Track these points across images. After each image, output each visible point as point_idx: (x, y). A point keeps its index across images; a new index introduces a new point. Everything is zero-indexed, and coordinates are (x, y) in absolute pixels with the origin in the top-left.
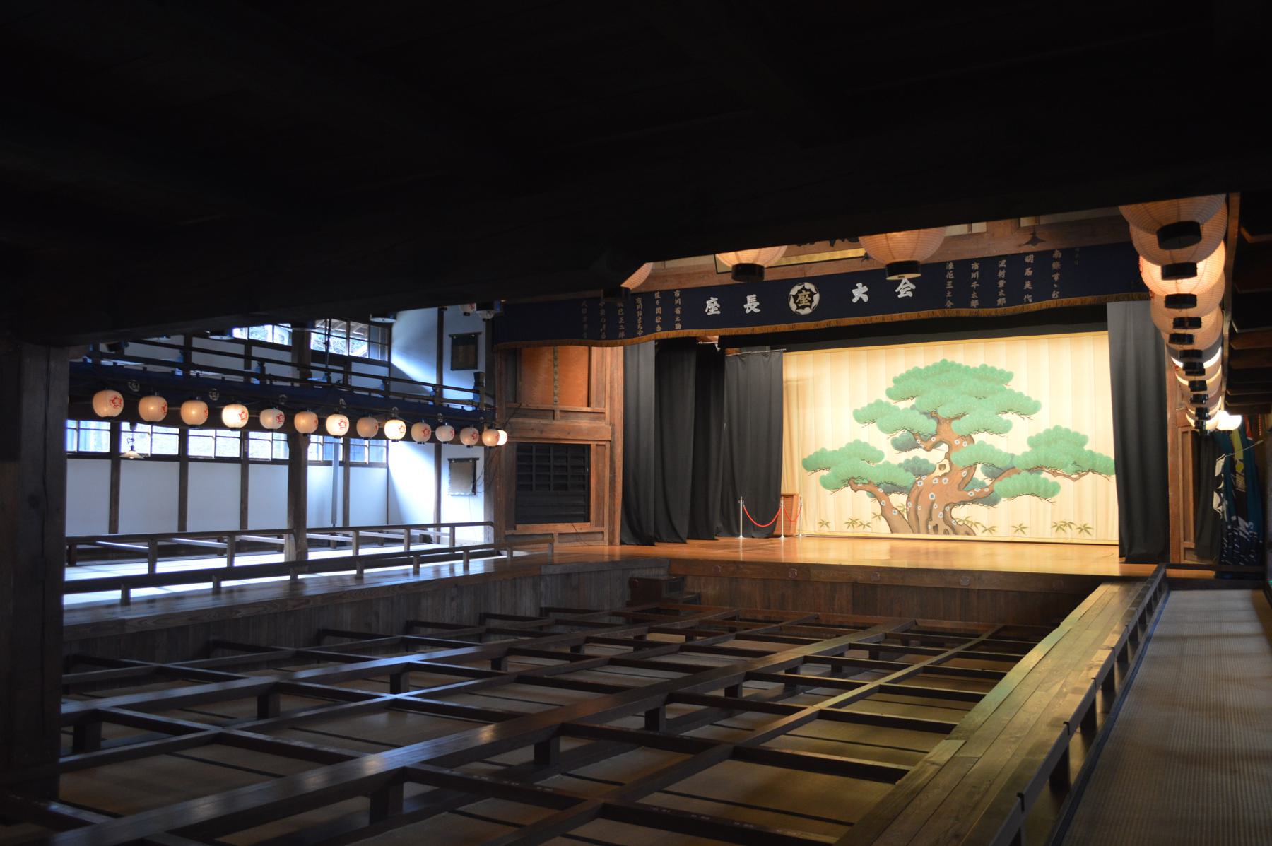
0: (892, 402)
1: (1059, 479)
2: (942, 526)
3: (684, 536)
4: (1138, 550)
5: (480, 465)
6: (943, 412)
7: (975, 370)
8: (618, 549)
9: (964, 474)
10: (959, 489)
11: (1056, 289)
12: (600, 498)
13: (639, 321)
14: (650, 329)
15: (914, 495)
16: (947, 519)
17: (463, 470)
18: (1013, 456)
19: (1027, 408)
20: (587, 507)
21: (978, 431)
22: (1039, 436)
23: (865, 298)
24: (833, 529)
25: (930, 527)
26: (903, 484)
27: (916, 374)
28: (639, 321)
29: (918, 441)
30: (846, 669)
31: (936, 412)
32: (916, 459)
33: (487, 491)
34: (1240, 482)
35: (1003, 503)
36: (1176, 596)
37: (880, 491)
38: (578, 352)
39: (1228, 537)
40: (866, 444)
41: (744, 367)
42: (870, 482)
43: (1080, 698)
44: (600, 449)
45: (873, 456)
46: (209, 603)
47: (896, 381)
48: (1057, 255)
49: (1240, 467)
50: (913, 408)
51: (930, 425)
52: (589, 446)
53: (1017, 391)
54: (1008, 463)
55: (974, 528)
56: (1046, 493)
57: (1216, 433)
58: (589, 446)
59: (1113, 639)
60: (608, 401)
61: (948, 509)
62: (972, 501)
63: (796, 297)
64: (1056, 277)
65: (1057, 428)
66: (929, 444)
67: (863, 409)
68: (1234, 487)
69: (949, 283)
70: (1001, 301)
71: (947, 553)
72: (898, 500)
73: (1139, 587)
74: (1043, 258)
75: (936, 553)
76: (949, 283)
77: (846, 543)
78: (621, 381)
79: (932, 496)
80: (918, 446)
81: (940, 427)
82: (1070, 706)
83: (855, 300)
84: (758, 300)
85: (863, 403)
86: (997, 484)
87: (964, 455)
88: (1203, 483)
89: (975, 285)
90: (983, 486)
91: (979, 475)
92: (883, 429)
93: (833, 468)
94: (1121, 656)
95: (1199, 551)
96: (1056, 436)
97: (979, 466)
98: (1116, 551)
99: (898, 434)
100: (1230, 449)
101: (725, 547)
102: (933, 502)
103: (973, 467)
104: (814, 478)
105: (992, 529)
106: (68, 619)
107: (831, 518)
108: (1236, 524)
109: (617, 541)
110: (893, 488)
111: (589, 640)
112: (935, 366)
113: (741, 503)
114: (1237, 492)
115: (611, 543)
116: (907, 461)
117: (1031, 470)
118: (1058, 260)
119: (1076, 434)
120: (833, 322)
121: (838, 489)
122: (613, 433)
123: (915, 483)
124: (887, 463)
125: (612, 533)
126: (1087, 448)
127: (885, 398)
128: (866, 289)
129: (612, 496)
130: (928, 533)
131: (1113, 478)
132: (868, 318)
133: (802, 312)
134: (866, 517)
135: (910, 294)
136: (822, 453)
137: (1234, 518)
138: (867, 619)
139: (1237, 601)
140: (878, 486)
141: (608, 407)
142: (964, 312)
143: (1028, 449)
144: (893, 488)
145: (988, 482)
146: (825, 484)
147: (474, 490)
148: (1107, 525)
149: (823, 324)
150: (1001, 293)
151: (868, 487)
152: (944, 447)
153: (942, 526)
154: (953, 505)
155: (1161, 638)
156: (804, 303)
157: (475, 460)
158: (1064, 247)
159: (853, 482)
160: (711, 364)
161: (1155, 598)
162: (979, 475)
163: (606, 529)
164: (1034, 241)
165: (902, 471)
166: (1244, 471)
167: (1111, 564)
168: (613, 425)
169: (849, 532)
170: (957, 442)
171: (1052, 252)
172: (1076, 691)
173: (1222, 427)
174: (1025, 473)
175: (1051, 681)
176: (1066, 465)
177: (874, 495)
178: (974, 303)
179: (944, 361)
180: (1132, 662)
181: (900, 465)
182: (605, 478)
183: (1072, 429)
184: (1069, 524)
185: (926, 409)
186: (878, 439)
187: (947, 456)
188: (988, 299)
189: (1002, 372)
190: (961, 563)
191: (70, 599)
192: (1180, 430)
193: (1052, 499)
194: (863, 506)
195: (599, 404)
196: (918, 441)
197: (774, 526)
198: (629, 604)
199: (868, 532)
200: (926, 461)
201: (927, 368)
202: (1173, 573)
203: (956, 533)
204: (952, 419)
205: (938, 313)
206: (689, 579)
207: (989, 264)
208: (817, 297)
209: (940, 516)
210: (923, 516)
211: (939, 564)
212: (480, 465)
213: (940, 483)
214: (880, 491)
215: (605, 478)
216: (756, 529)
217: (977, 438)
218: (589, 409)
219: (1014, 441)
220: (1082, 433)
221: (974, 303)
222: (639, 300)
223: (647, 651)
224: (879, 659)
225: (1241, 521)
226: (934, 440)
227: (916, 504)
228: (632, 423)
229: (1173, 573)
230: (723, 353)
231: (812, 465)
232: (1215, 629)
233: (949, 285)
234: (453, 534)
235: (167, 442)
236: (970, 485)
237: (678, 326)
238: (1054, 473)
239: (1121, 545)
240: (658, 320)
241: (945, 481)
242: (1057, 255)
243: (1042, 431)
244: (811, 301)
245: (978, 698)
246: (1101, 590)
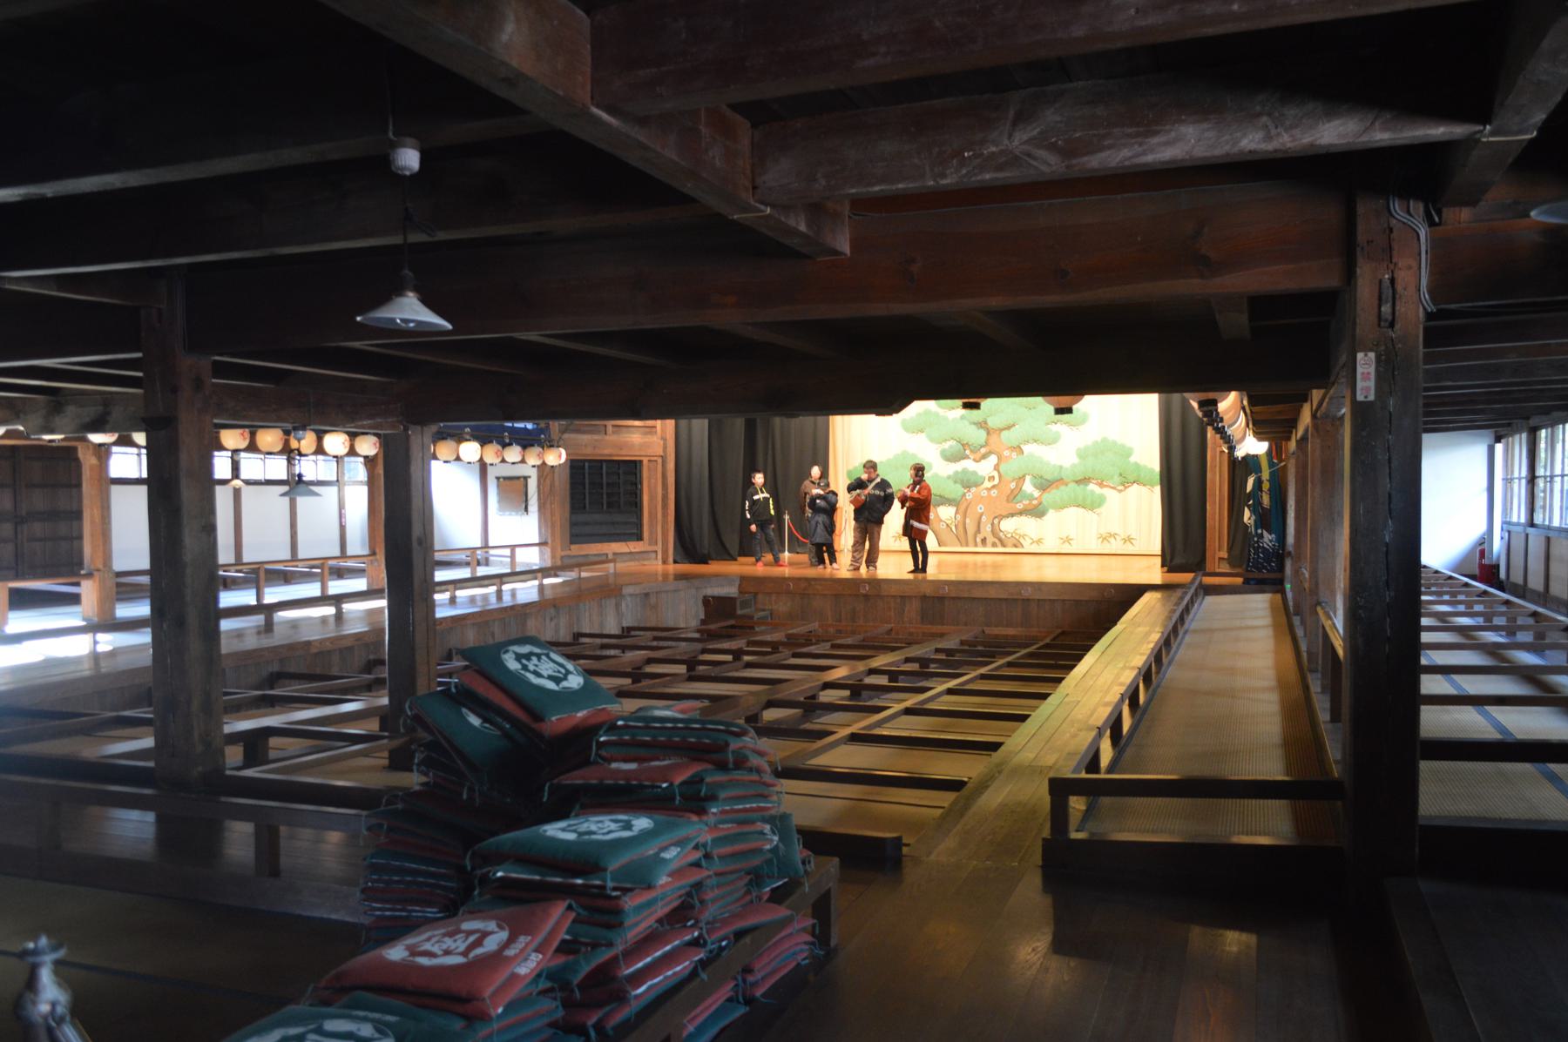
1: (1106, 491)
2: (991, 539)
3: (734, 550)
4: (1178, 560)
5: (533, 485)
8: (672, 568)
9: (1013, 485)
15: (962, 508)
16: (995, 532)
17: (514, 491)
20: (640, 525)
26: (952, 496)
30: (865, 694)
32: (965, 471)
33: (541, 507)
34: (1266, 500)
35: (1051, 514)
36: (1209, 600)
43: (1109, 709)
46: (331, 632)
49: (1266, 486)
51: (981, 436)
56: (1092, 505)
57: (1247, 458)
59: (1156, 636)
62: (1021, 513)
65: (1105, 440)
66: (978, 456)
68: (1261, 504)
71: (995, 566)
73: (1179, 593)
75: (984, 566)
79: (980, 508)
80: (967, 457)
82: (1103, 714)
87: (1012, 467)
88: (1236, 498)
90: (1031, 498)
91: (1028, 487)
92: (932, 440)
94: (1167, 643)
95: (1231, 561)
96: (1103, 448)
98: (1159, 560)
99: (946, 445)
100: (1258, 470)
103: (1023, 478)
105: (1039, 542)
106: (226, 647)
108: (1261, 536)
111: (650, 661)
113: (787, 517)
115: (665, 562)
117: (1078, 482)
122: (665, 448)
125: (665, 552)
126: (1132, 459)
129: (665, 515)
131: (1158, 489)
138: (945, 628)
139: (1259, 604)
143: (1076, 460)
145: (1036, 494)
147: (526, 509)
148: (1152, 539)
152: (993, 459)
153: (991, 539)
154: (1001, 517)
155: (1195, 631)
157: (526, 478)
161: (1192, 601)
162: (1028, 487)
163: (659, 548)
165: (951, 482)
167: (1153, 573)
168: (664, 439)
170: (1006, 453)
172: (1106, 704)
173: (1252, 452)
175: (1101, 678)
180: (1165, 660)
184: (1114, 536)
187: (996, 468)
190: (1008, 575)
191: (226, 625)
198: (703, 622)
200: (975, 473)
202: (1208, 580)
203: (1004, 546)
206: (760, 597)
209: (989, 528)
210: (971, 529)
211: (987, 576)
212: (533, 485)
217: (1026, 448)
223: (645, 683)
224: (952, 662)
227: (965, 516)
228: (684, 436)
229: (1208, 580)
232: (1238, 623)
234: (513, 556)
235: (277, 468)
238: (1101, 485)
239: (1163, 555)
241: (994, 493)
245: (1060, 680)
246: (1148, 597)
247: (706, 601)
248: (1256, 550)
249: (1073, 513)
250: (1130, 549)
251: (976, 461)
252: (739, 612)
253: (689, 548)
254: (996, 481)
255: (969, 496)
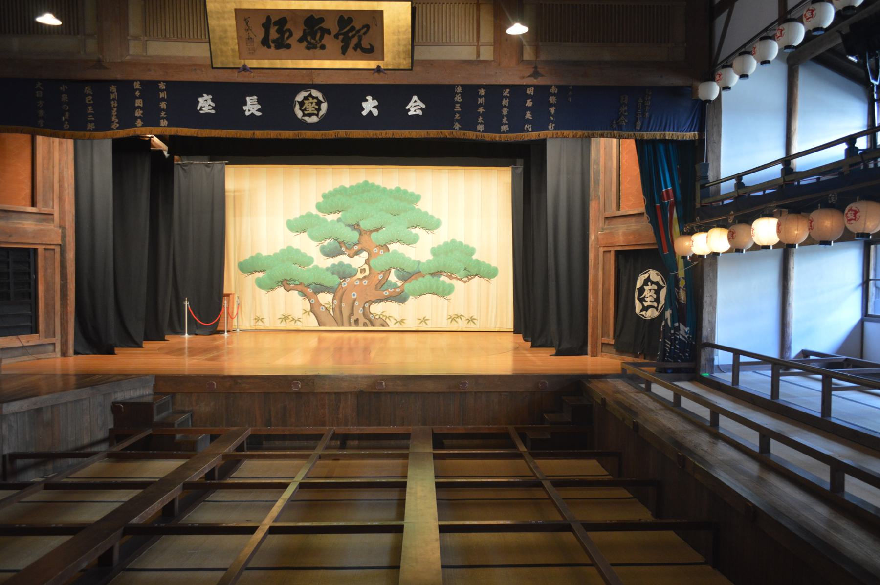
0: (321, 215)
1: (454, 282)
2: (362, 320)
4: (565, 345)
6: (365, 225)
7: (391, 191)
9: (380, 276)
10: (376, 289)
11: (552, 122)
12: (50, 307)
13: (114, 112)
14: (103, 125)
15: (339, 294)
16: (365, 315)
18: (419, 262)
19: (431, 225)
21: (392, 242)
22: (439, 247)
23: (375, 113)
24: (268, 324)
25: (352, 321)
27: (342, 191)
28: (114, 112)
29: (343, 249)
31: (358, 225)
32: (341, 264)
34: (683, 296)
35: (411, 300)
37: (310, 291)
38: (18, 141)
39: (671, 340)
40: (298, 251)
41: (191, 173)
42: (301, 283)
44: (48, 253)
45: (304, 261)
47: (325, 196)
48: (554, 90)
50: (339, 220)
51: (354, 236)
52: (35, 250)
53: (423, 210)
54: (415, 268)
55: (387, 321)
56: (443, 292)
58: (35, 250)
60: (56, 201)
61: (367, 305)
62: (387, 299)
63: (302, 104)
64: (552, 110)
65: (453, 241)
66: (352, 252)
67: (296, 219)
69: (458, 106)
70: (504, 128)
72: (326, 298)
74: (542, 91)
76: (458, 106)
77: (282, 336)
78: (72, 181)
79: (354, 295)
80: (343, 253)
81: (361, 238)
83: (364, 113)
84: (259, 102)
85: (296, 214)
86: (407, 285)
87: (380, 262)
89: (481, 110)
90: (395, 286)
91: (393, 278)
92: (313, 238)
93: (268, 271)
96: (452, 247)
97: (393, 271)
101: (194, 351)
102: (355, 300)
103: (389, 270)
104: (251, 279)
105: (401, 321)
107: (266, 315)
108: (678, 329)
109: (71, 351)
110: (321, 288)
112: (358, 186)
113: (186, 303)
114: (679, 303)
115: (64, 354)
116: (334, 265)
118: (554, 95)
119: (467, 247)
120: (342, 134)
121: (272, 289)
122: (64, 236)
123: (340, 284)
124: (317, 267)
125: (64, 344)
126: (474, 257)
127: (315, 211)
128: (376, 103)
130: (350, 325)
132: (378, 132)
133: (309, 120)
134: (297, 313)
135: (420, 113)
136: (257, 258)
137: (676, 324)
140: (308, 286)
141: (56, 208)
142: (471, 135)
143: (431, 257)
144: (321, 288)
145: (399, 284)
146: (260, 285)
149: (331, 134)
150: (505, 120)
151: (300, 288)
152: (365, 255)
156: (310, 111)
157: (54, 344)
158: (562, 83)
159: (286, 283)
160: (162, 170)
162: (393, 278)
164: (536, 74)
166: (685, 286)
168: (63, 228)
169: (282, 326)
171: (550, 87)
174: (428, 277)
176: (459, 271)
177: (304, 295)
178: (481, 127)
179: (366, 182)
181: (327, 269)
182: (54, 285)
183: (464, 243)
184: (460, 317)
185: (350, 222)
186: (309, 247)
187: (367, 262)
188: (493, 126)
189: (412, 194)
192: (601, 250)
193: (448, 297)
194: (295, 304)
195: (46, 204)
196: (343, 249)
197: (217, 324)
199: (299, 326)
200: (349, 266)
201: (352, 187)
203: (373, 325)
204: (371, 231)
205: (447, 133)
207: (494, 91)
208: (324, 107)
209: (361, 311)
210: (346, 313)
213: (361, 284)
214: (310, 291)
215: (54, 285)
216: (199, 327)
217: (392, 247)
218: (34, 210)
219: (420, 251)
220: (471, 246)
221: (481, 127)
222: (113, 88)
225: (682, 327)
226: (356, 248)
227: (341, 301)
230: (171, 158)
231: (247, 268)
233: (458, 108)
236: (385, 287)
237: (164, 123)
238: (450, 277)
240: (139, 113)
241: (365, 282)
242: (554, 90)
243: (442, 243)
244: (319, 110)
247: (116, 408)
248: (673, 342)
249: (428, 299)
250: (472, 327)
251: (349, 256)
252: (157, 418)
253: (93, 337)
254: (367, 273)
255: (344, 285)
